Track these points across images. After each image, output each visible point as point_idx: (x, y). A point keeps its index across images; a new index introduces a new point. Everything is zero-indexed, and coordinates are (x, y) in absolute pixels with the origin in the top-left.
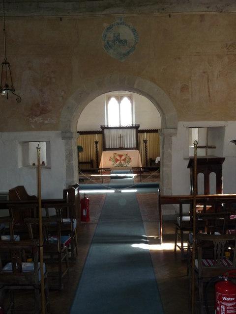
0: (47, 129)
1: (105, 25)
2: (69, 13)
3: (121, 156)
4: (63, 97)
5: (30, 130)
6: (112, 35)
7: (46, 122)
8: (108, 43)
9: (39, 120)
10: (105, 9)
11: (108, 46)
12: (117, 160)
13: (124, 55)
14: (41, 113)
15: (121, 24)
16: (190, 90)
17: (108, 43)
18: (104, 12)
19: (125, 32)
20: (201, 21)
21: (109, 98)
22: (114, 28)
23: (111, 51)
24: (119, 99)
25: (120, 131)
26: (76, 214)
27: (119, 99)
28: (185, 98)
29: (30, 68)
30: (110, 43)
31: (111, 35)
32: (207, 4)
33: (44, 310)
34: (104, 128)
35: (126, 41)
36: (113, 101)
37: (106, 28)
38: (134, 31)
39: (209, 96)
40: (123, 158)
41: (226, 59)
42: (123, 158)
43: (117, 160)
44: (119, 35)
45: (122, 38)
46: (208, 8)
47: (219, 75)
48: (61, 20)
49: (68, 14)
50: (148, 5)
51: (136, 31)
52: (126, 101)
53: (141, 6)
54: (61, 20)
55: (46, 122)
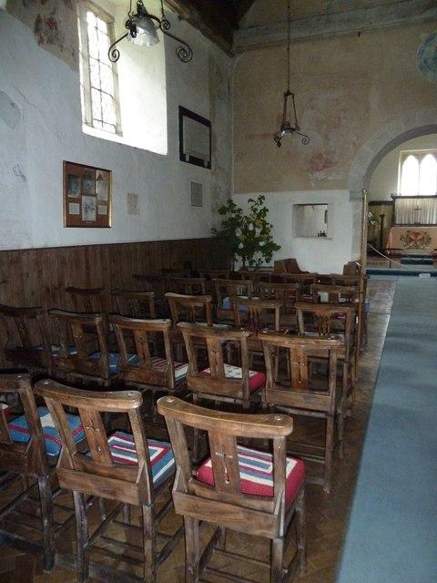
0: (331, 188)
3: (417, 234)
4: (354, 144)
5: (311, 189)
7: (330, 178)
9: (321, 175)
12: (411, 240)
14: (324, 167)
17: (425, 62)
21: (405, 157)
24: (420, 157)
25: (418, 202)
27: (420, 157)
29: (313, 108)
33: (263, 430)
34: (395, 198)
36: (411, 160)
37: (424, 40)
40: (420, 237)
42: (420, 237)
43: (411, 240)
48: (279, 144)
52: (429, 158)
54: (279, 144)
55: (330, 178)
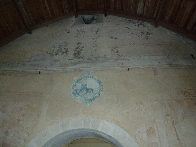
1: (76, 78)
2: (46, 68)
6: (80, 85)
8: (76, 91)
10: (75, 65)
11: (76, 93)
13: (90, 100)
15: (88, 77)
16: (157, 132)
18: (74, 67)
19: (92, 83)
20: (155, 75)
22: (82, 80)
23: (79, 97)
26: (190, 9)
28: (152, 141)
30: (78, 91)
31: (79, 86)
32: (158, 60)
35: (92, 90)
38: (99, 82)
39: (179, 139)
41: (163, 117)
44: (86, 85)
45: (88, 87)
46: (159, 62)
47: (183, 118)
48: (39, 74)
49: (46, 69)
50: (110, 61)
51: (100, 82)
53: (104, 62)
54: (39, 74)
